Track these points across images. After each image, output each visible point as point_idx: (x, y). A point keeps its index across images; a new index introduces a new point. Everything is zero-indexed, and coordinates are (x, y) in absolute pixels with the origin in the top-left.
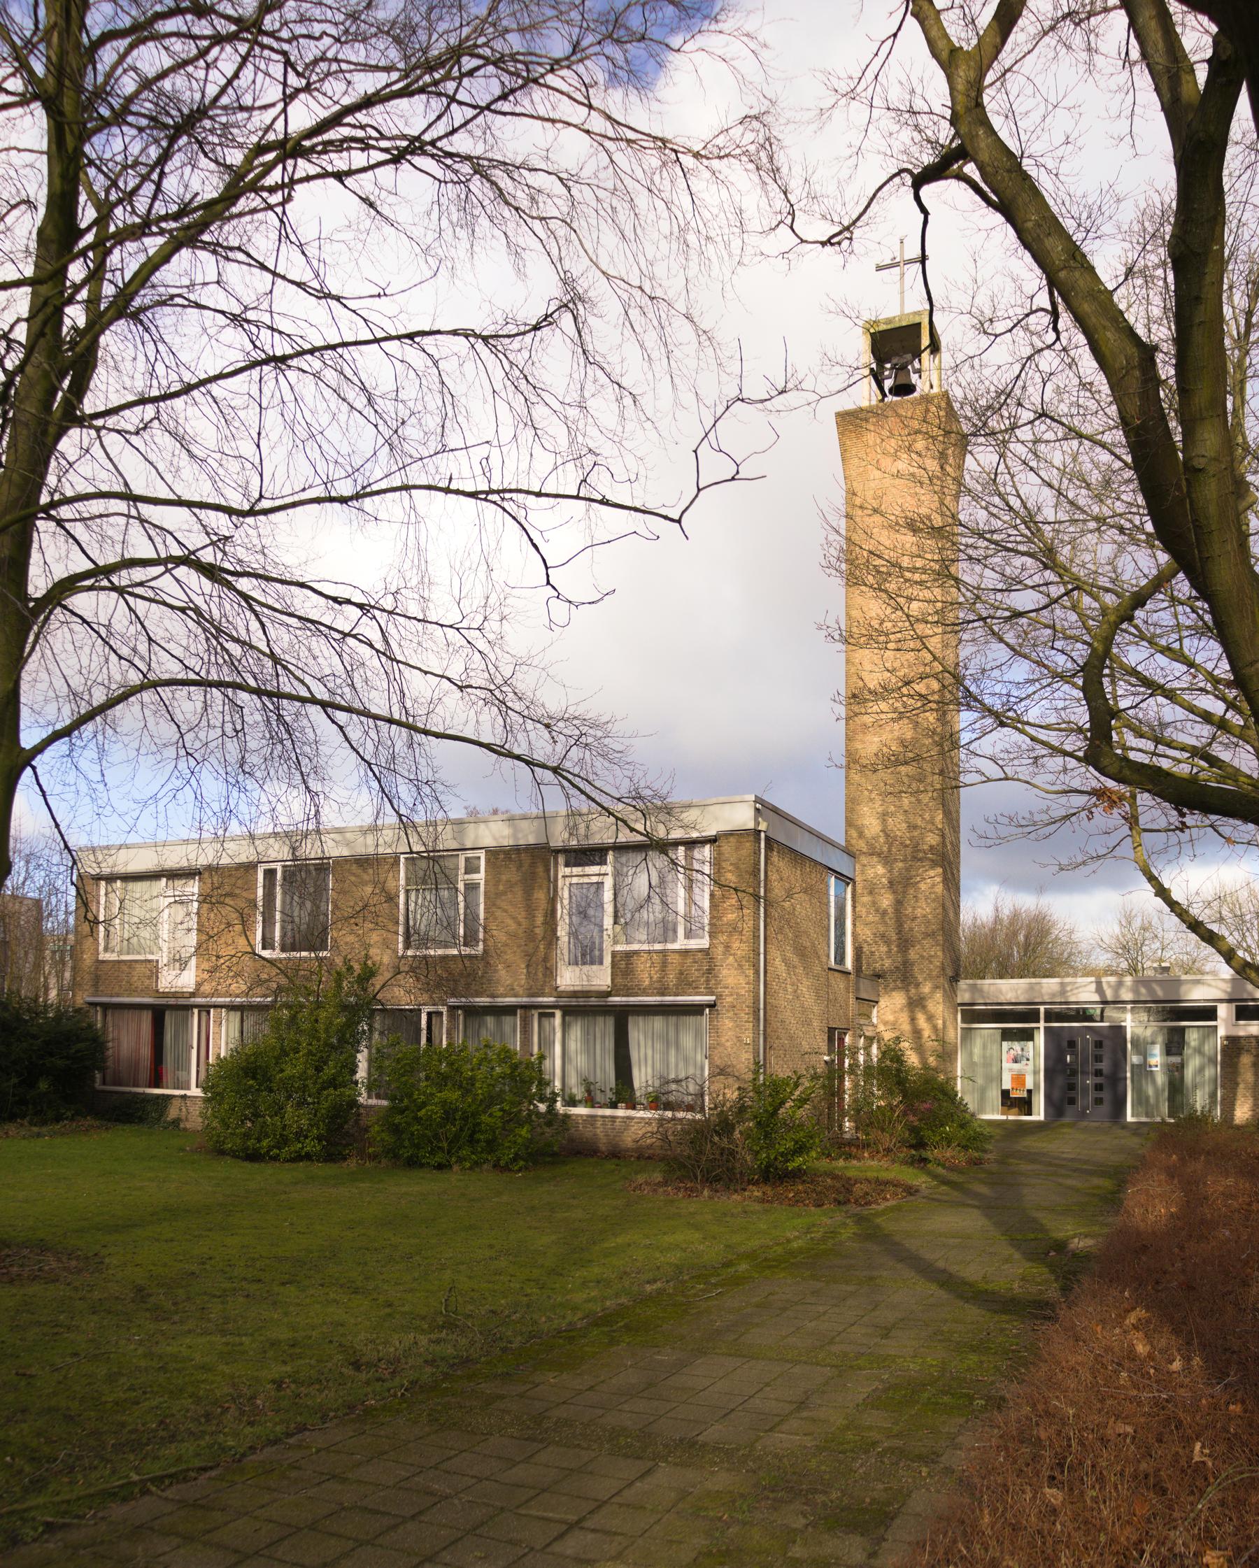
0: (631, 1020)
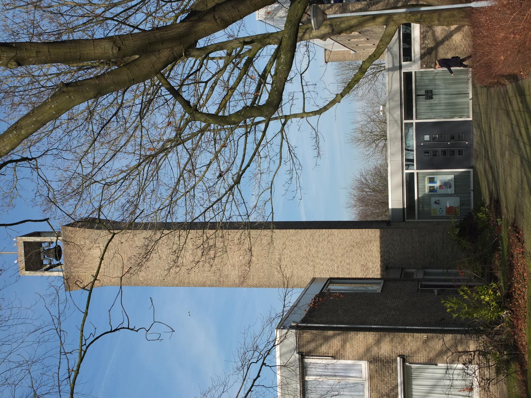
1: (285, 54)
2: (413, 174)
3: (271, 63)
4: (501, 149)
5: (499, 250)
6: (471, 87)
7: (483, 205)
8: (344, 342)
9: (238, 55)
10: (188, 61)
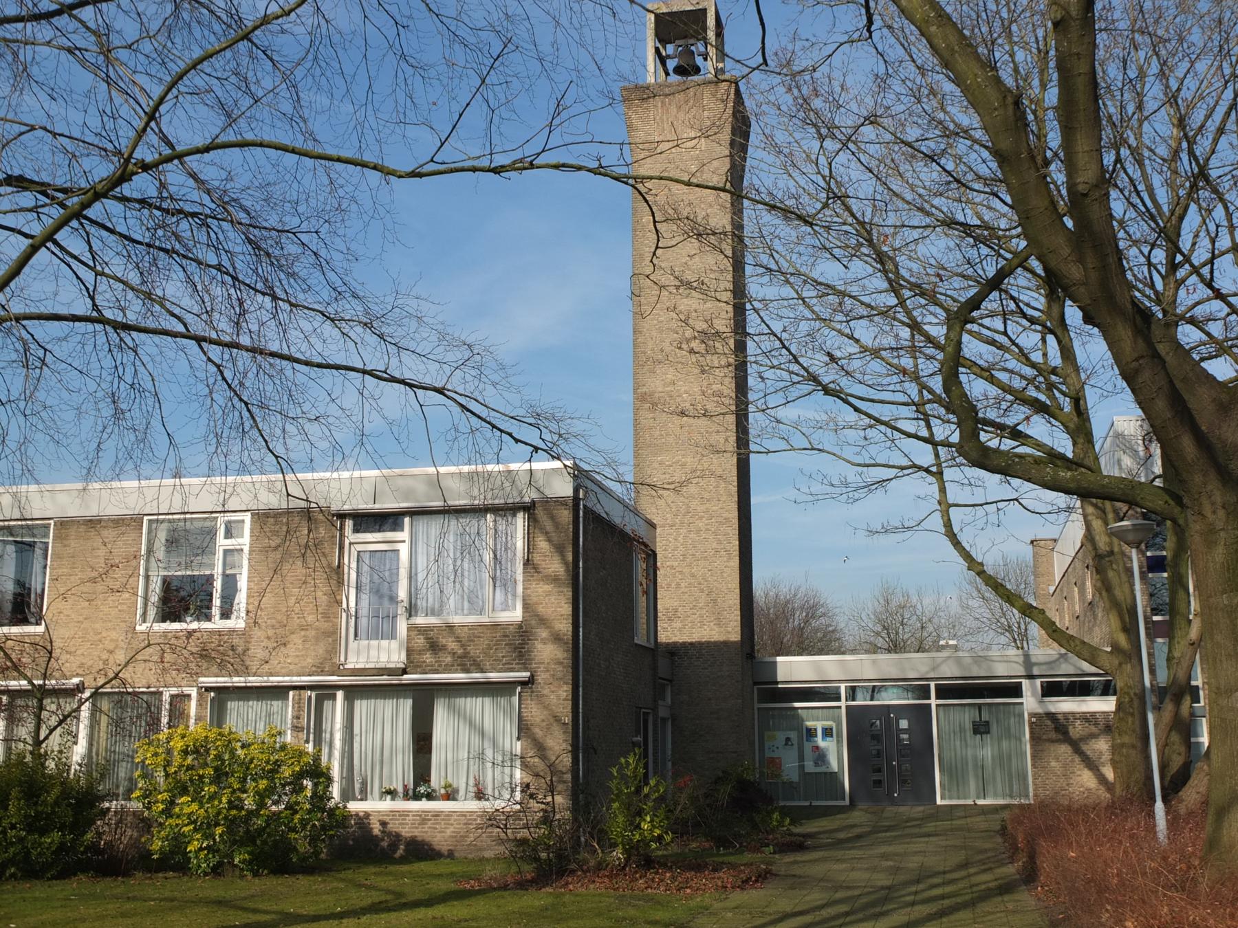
0: (231, 705)
1: (1073, 479)
2: (839, 699)
3: (1039, 445)
4: (897, 855)
5: (718, 848)
6: (1001, 802)
7: (793, 822)
8: (555, 580)
9: (1051, 387)
10: (1036, 295)
